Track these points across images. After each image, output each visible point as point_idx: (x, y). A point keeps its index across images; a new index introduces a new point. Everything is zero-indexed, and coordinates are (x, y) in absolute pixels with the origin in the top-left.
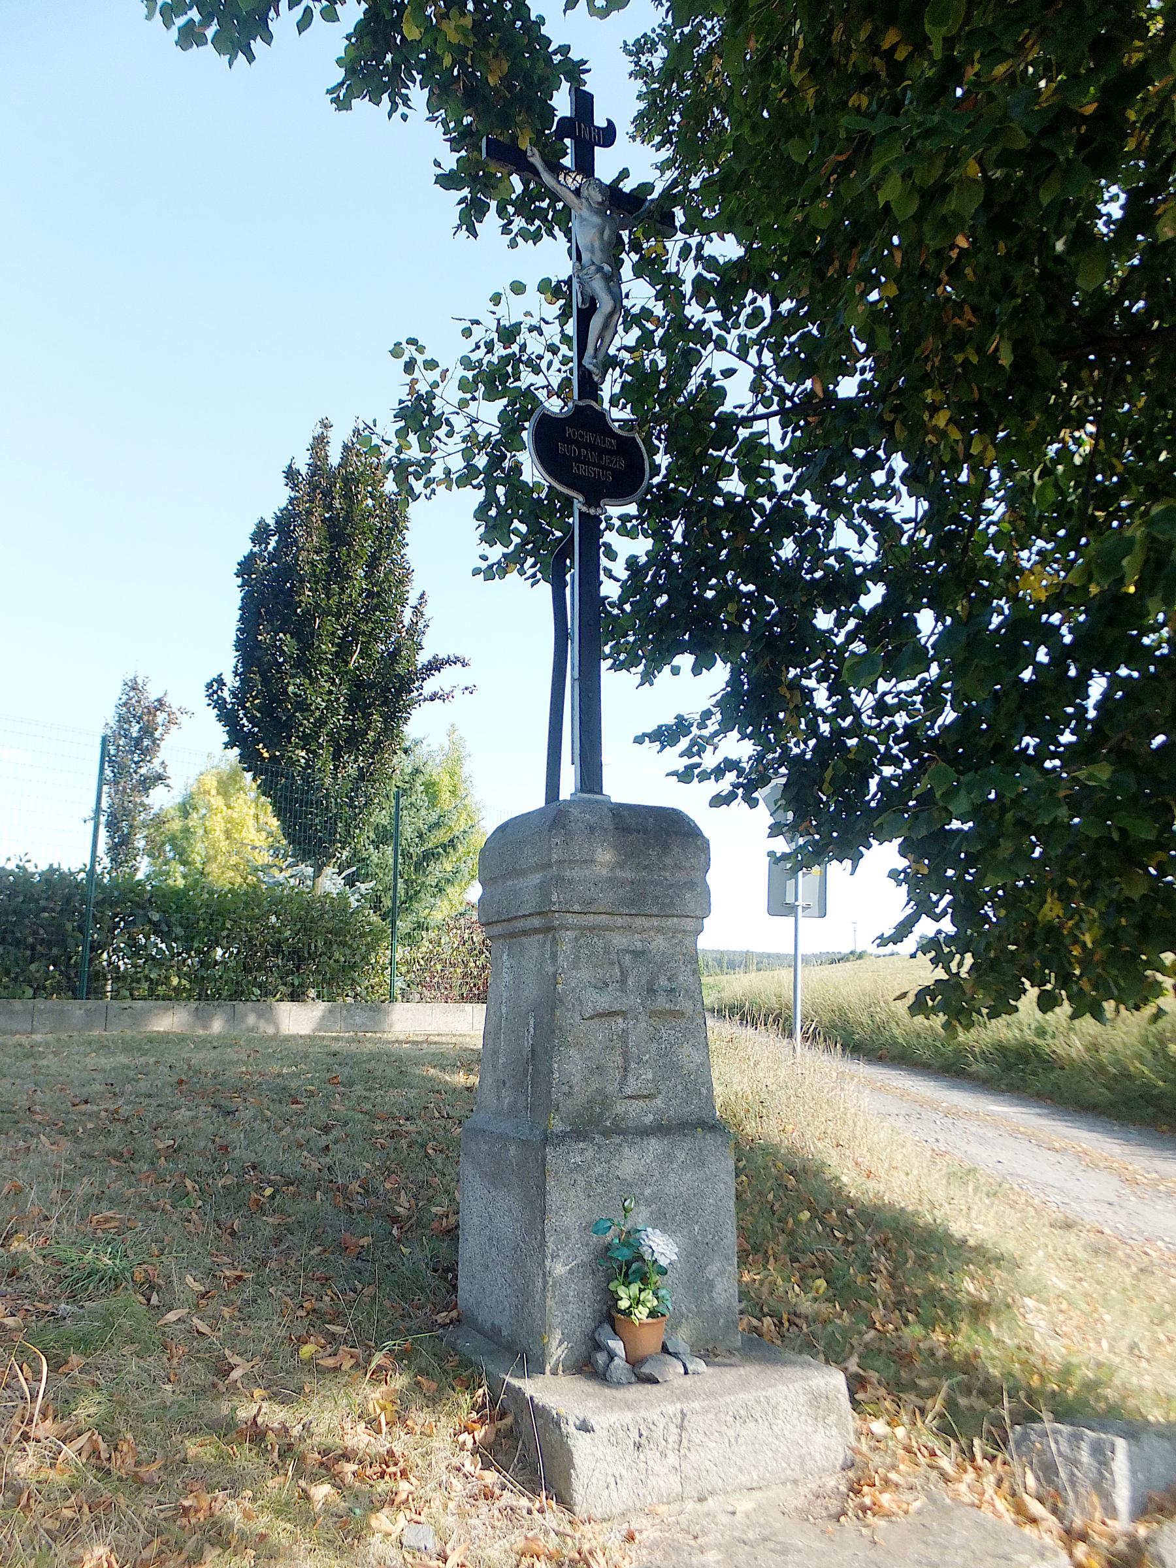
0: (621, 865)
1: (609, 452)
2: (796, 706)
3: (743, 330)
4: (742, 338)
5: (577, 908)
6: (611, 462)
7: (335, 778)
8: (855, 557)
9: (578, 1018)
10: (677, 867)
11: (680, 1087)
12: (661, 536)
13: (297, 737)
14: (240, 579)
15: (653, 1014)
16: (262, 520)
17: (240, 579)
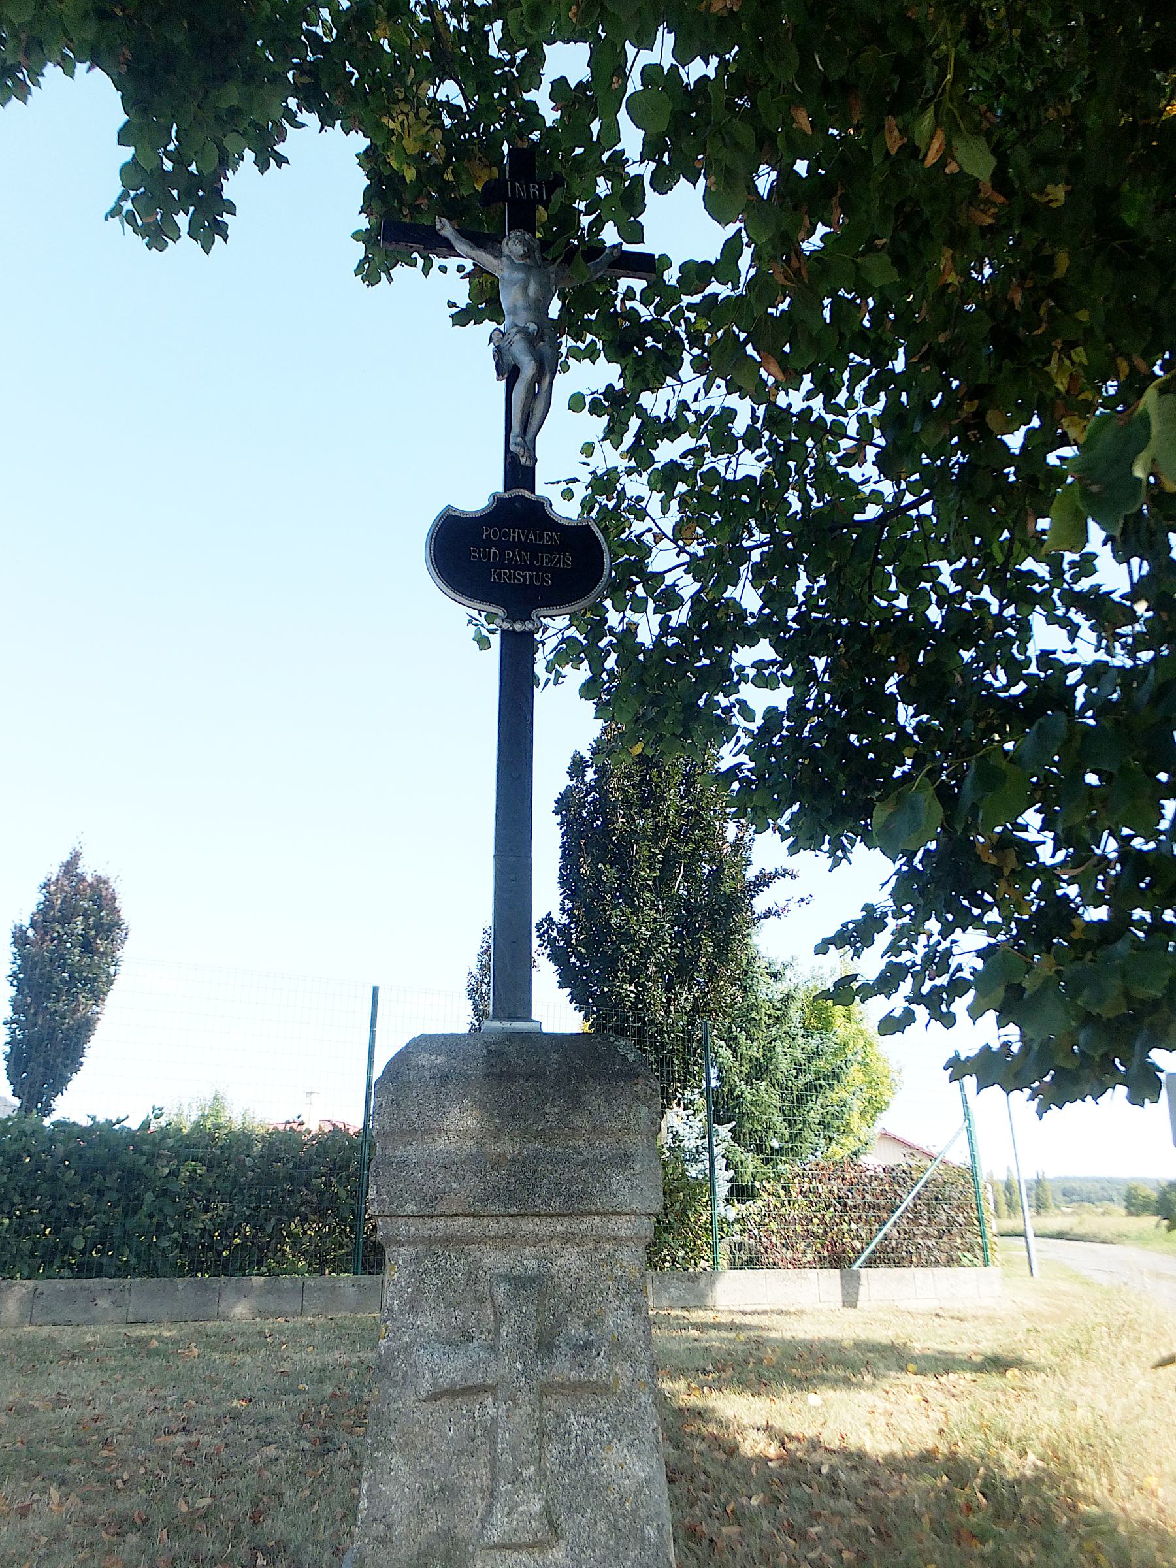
0: (496, 1135)
1: (550, 549)
2: (1013, 871)
3: (862, 408)
4: (862, 418)
5: (411, 1208)
6: (551, 561)
7: (668, 1011)
8: (1067, 659)
9: (409, 1398)
10: (598, 1130)
11: (602, 1526)
12: (804, 679)
13: (626, 970)
14: (559, 817)
15: (546, 1389)
16: (576, 753)
17: (559, 817)
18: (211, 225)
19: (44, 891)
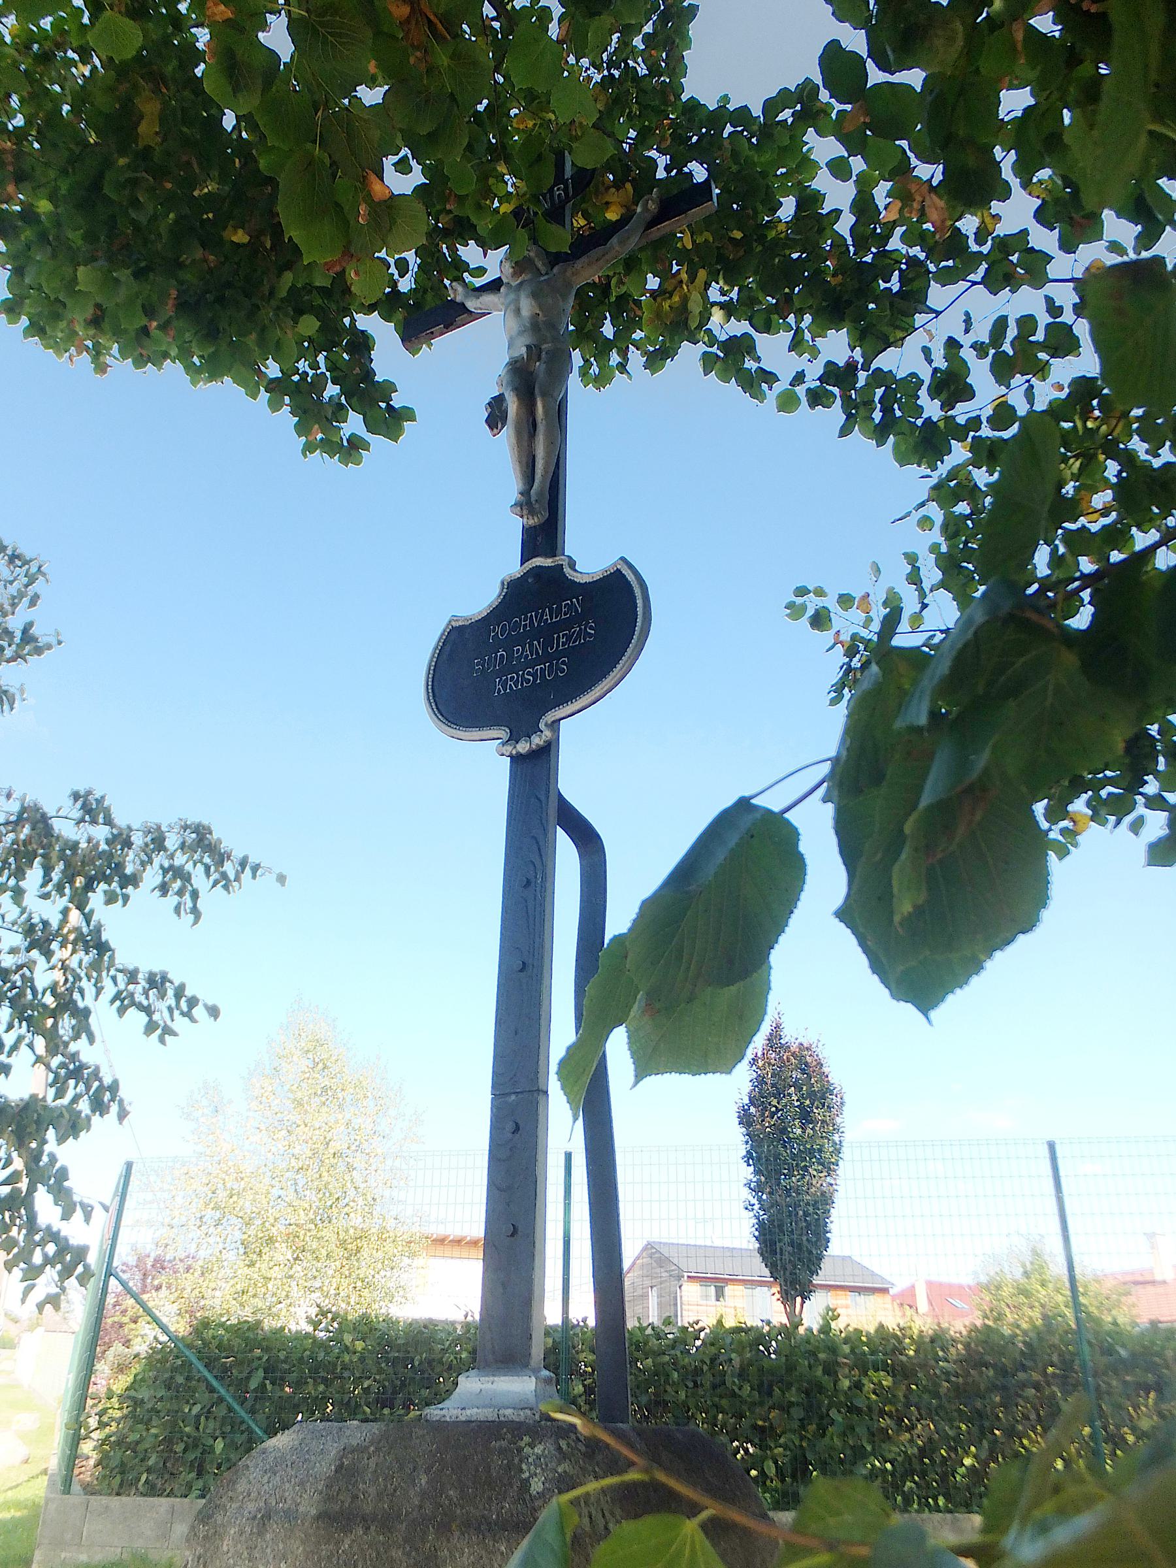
6: (569, 638)
18: (407, 414)
19: (754, 1068)
